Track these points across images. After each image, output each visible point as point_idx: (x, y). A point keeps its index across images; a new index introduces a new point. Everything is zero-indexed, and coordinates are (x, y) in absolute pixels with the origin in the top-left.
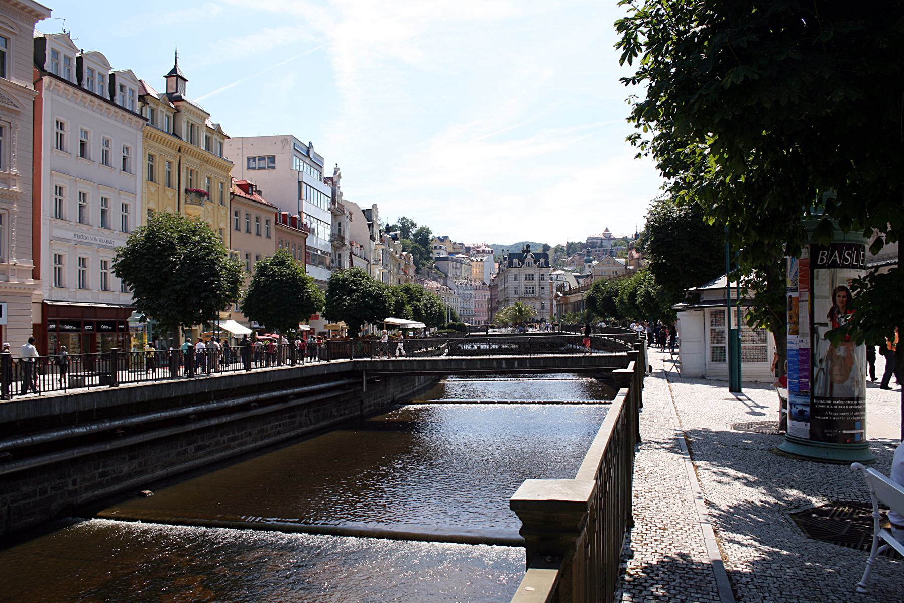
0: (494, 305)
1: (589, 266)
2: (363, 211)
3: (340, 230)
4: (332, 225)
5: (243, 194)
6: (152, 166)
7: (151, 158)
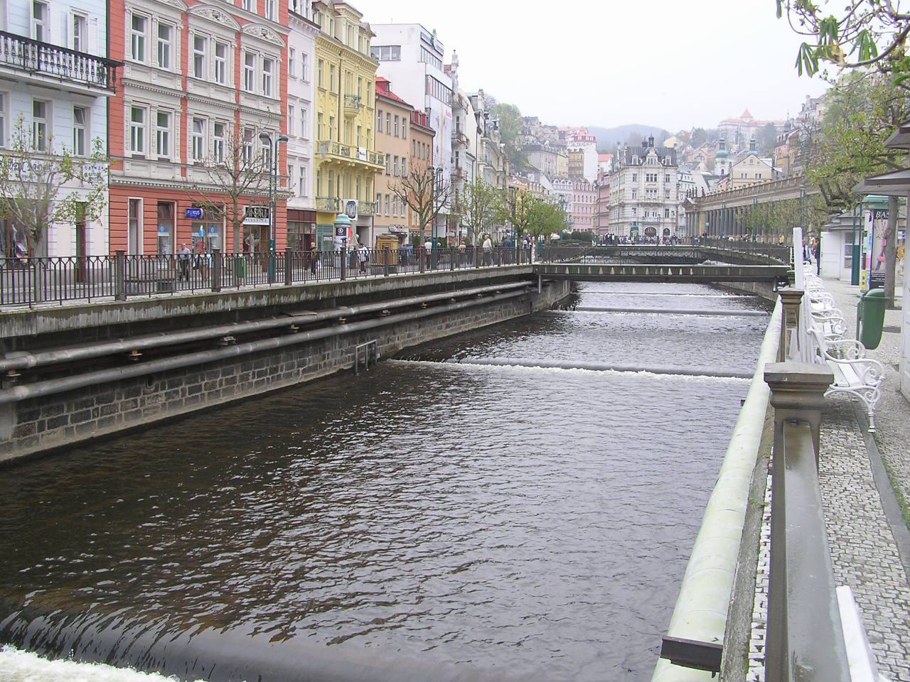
0: (604, 210)
3: (458, 125)
6: (81, 131)
7: (321, 61)
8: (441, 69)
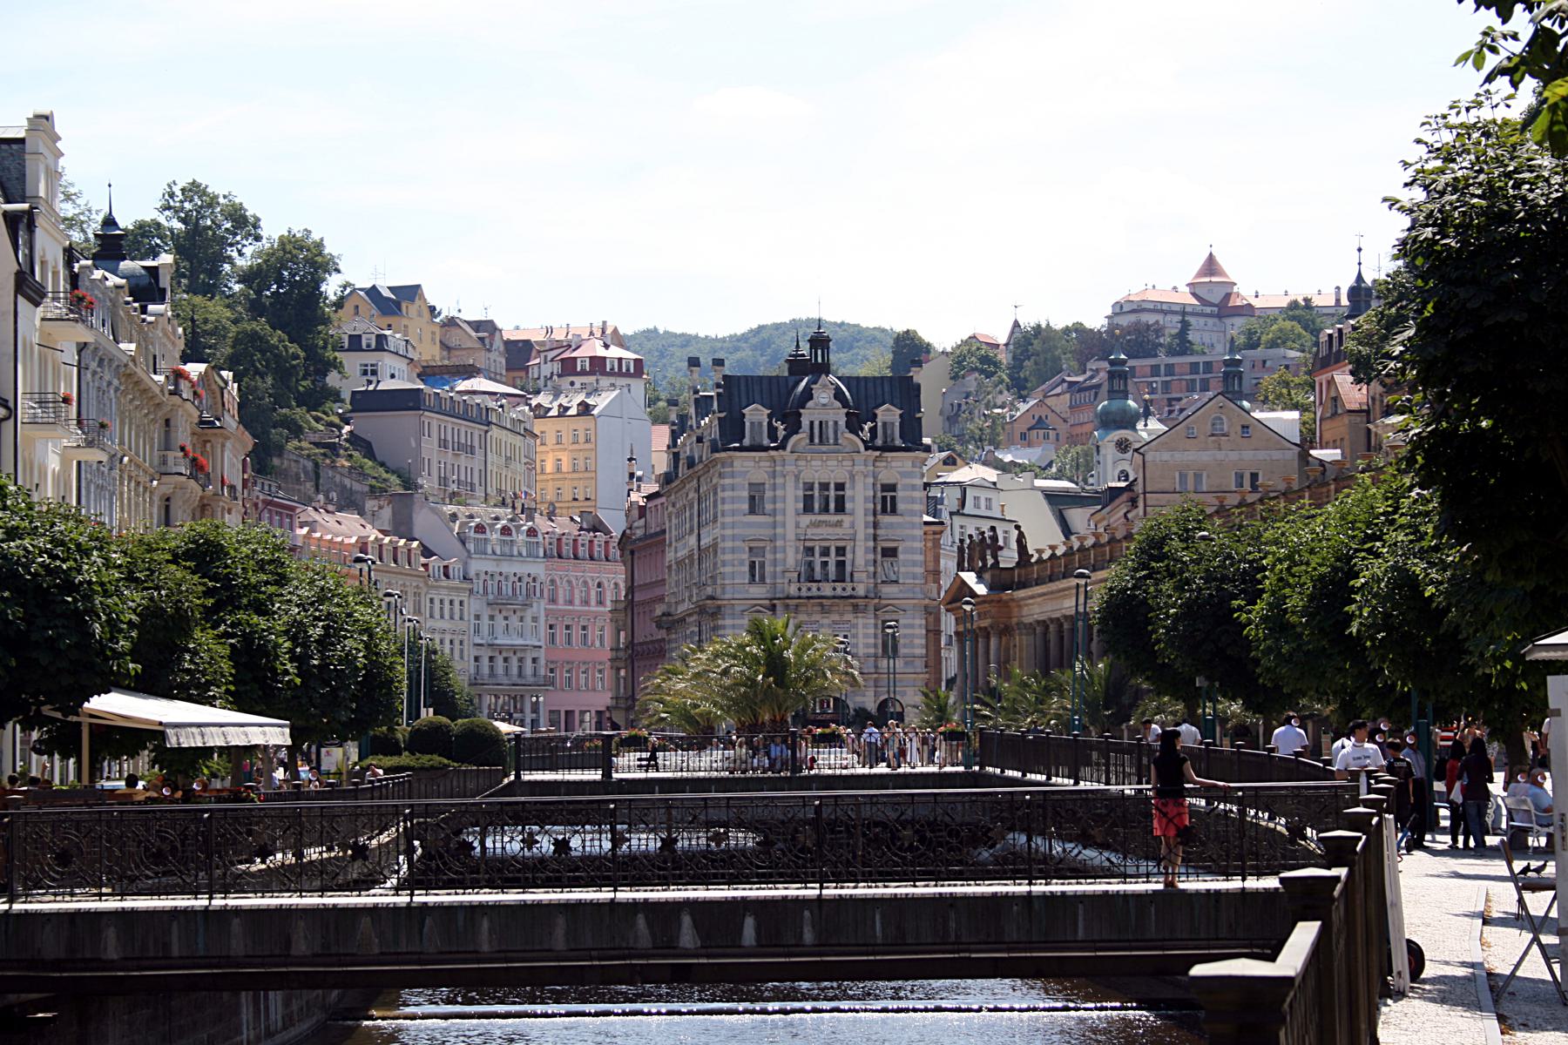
0: (647, 631)
1: (1123, 446)
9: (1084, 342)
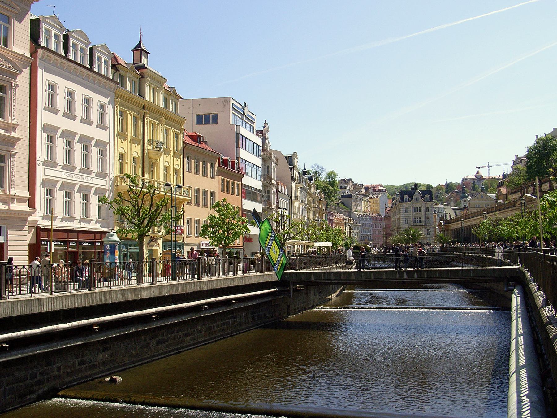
1: (465, 201)
2: (286, 158)
4: (263, 168)
5: (193, 143)
8: (253, 133)
9: (458, 186)
